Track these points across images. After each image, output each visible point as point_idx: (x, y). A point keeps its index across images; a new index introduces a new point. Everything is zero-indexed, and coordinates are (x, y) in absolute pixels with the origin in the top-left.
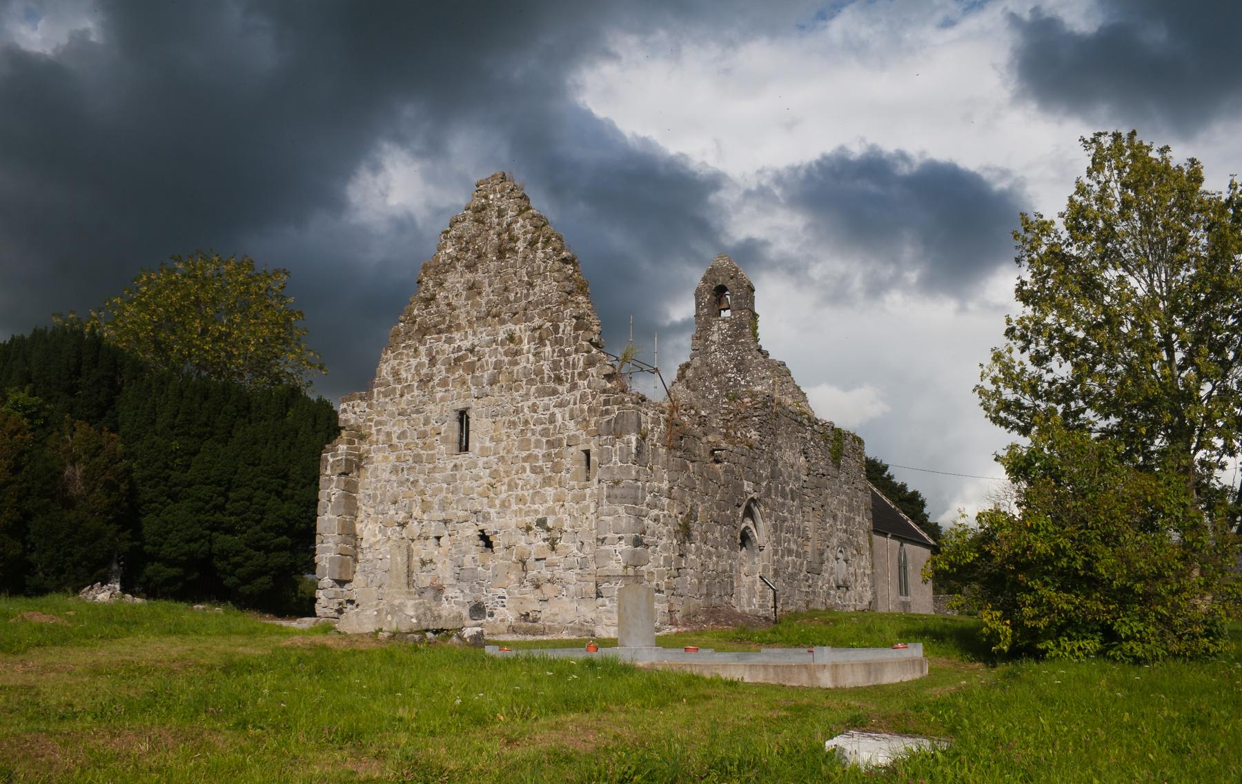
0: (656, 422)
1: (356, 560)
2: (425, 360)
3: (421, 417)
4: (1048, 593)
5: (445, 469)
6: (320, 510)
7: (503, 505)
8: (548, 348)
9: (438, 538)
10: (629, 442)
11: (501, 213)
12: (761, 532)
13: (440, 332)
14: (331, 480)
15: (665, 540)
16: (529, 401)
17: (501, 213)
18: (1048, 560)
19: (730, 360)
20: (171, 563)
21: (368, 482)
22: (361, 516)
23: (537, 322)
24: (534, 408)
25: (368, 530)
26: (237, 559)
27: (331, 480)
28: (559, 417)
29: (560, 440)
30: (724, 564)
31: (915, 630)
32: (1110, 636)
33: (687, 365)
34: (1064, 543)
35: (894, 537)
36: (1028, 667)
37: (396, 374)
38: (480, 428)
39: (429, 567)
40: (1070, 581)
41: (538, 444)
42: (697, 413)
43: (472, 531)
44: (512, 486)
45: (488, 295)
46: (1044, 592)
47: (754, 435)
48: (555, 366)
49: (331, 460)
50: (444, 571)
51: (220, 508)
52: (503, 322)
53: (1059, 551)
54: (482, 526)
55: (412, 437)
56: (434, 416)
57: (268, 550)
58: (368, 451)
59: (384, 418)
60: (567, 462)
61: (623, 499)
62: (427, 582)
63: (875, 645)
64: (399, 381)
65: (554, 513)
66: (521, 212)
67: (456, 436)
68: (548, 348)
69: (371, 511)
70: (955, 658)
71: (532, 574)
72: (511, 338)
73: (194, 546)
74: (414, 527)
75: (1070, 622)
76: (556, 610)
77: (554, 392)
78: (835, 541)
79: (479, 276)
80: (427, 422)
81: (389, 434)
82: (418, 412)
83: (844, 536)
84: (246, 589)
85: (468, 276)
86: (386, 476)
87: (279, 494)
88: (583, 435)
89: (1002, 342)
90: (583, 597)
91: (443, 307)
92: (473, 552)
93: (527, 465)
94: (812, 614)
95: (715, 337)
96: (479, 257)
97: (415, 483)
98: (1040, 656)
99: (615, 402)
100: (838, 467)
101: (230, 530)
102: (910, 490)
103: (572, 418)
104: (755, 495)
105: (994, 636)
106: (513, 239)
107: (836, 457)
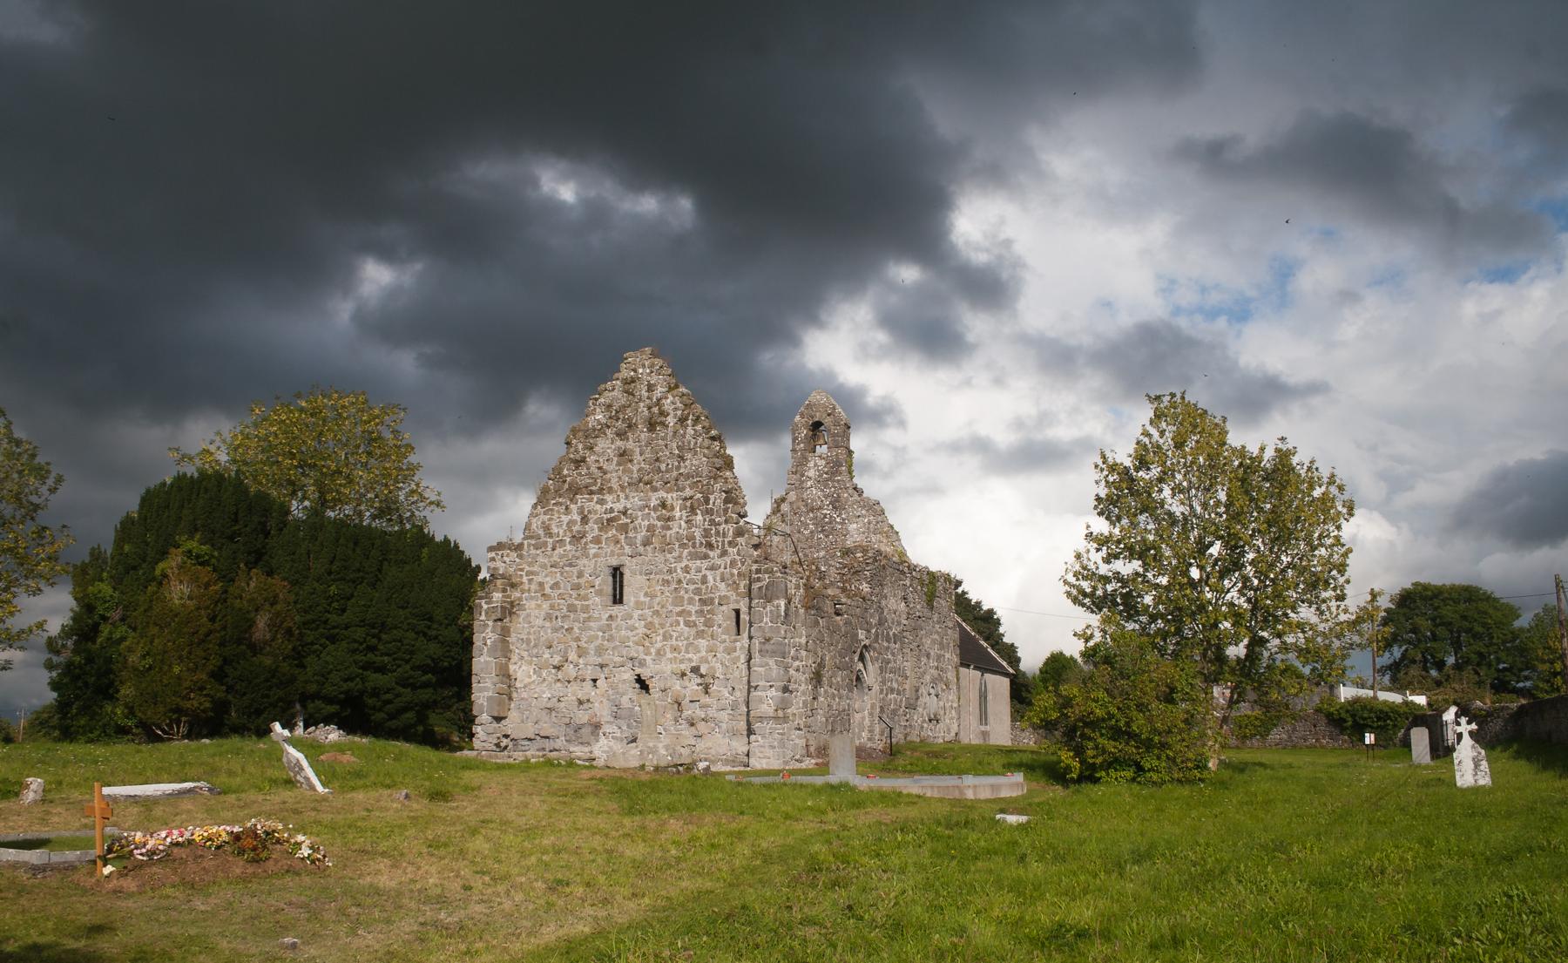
0: (797, 587)
1: (510, 699)
2: (577, 518)
3: (575, 570)
4: (1102, 741)
5: (600, 619)
6: (475, 652)
7: (658, 653)
8: (699, 517)
9: (595, 681)
10: (778, 606)
11: (651, 388)
12: (871, 675)
13: (591, 493)
14: (486, 626)
15: (803, 687)
16: (680, 561)
17: (651, 388)
18: (1103, 720)
19: (826, 497)
20: (330, 701)
21: (520, 627)
22: (515, 658)
23: (688, 492)
24: (686, 570)
25: (522, 672)
26: (388, 696)
27: (486, 626)
28: (710, 578)
29: (712, 599)
30: (844, 704)
31: (1011, 760)
32: (1140, 769)
33: (783, 500)
34: (1114, 710)
35: (976, 668)
36: (1088, 788)
37: (547, 529)
38: (634, 584)
39: (586, 706)
40: (1117, 734)
41: (691, 601)
42: (818, 569)
43: (628, 676)
44: (666, 637)
45: (639, 463)
46: (1100, 740)
47: (865, 587)
48: (706, 533)
49: (485, 607)
50: (602, 710)
51: (372, 649)
52: (655, 490)
53: (1111, 716)
54: (638, 671)
55: (565, 588)
56: (588, 571)
57: (414, 687)
58: (520, 599)
59: (535, 569)
60: (719, 618)
61: (773, 653)
62: (585, 719)
63: (986, 774)
64: (551, 535)
65: (707, 662)
66: (670, 389)
67: (609, 589)
68: (699, 517)
69: (525, 654)
70: (1042, 782)
71: (686, 713)
72: (663, 505)
73: (351, 685)
74: (570, 670)
75: (1116, 760)
76: (710, 744)
77: (706, 557)
78: (928, 678)
79: (630, 445)
80: (580, 575)
81: (541, 584)
82: (571, 565)
83: (935, 672)
84: (393, 724)
85: (619, 443)
86: (539, 622)
87: (425, 635)
88: (733, 596)
89: (1082, 545)
90: (734, 733)
91: (593, 469)
92: (631, 693)
93: (681, 619)
94: (912, 747)
95: (811, 473)
96: (630, 426)
97: (569, 630)
98: (1096, 781)
99: (766, 572)
100: (932, 608)
101: (381, 669)
102: (985, 608)
103: (723, 580)
104: (867, 642)
105: (1068, 769)
106: (663, 413)
107: (930, 599)
